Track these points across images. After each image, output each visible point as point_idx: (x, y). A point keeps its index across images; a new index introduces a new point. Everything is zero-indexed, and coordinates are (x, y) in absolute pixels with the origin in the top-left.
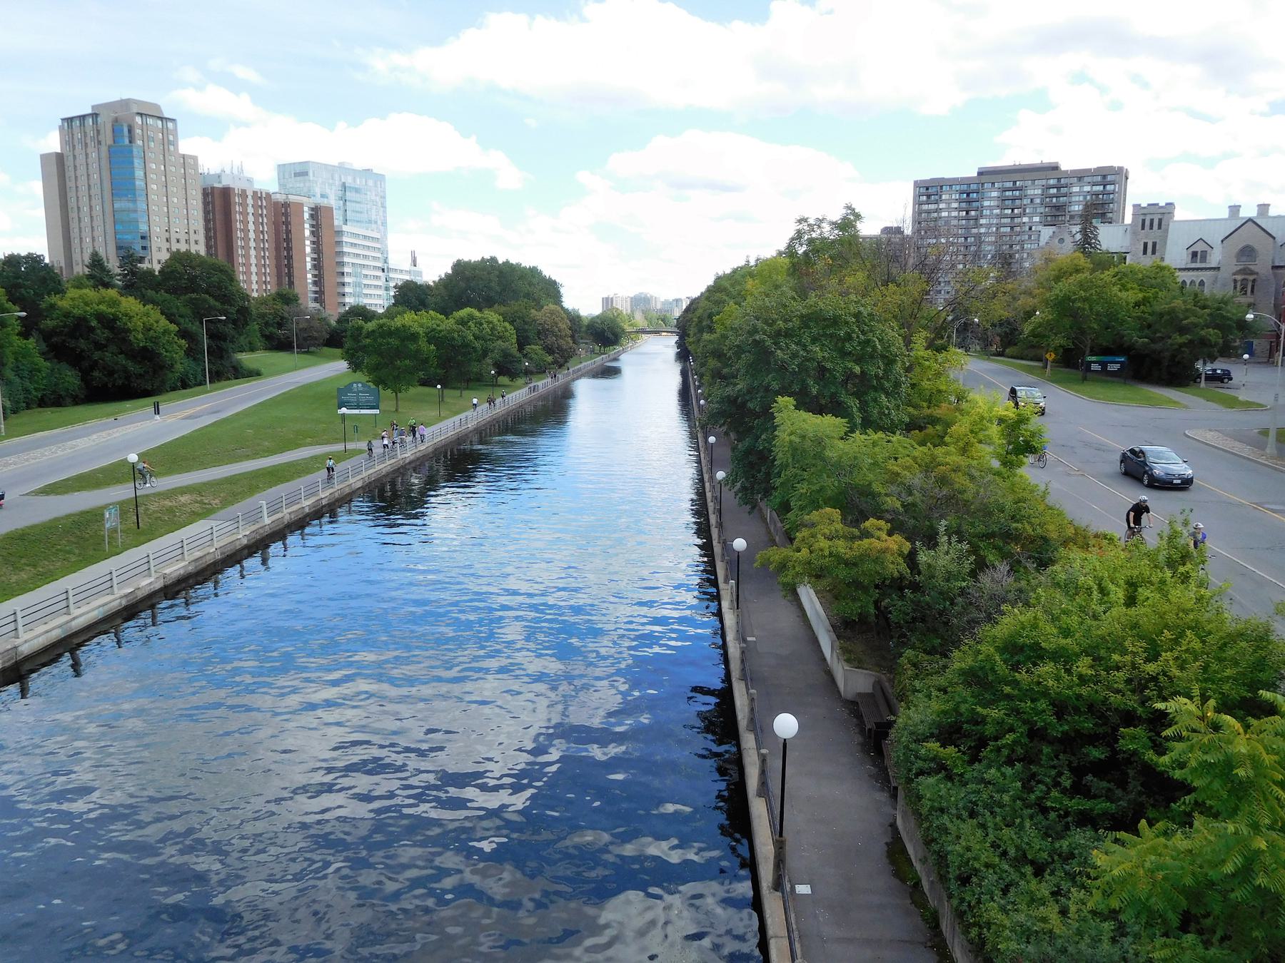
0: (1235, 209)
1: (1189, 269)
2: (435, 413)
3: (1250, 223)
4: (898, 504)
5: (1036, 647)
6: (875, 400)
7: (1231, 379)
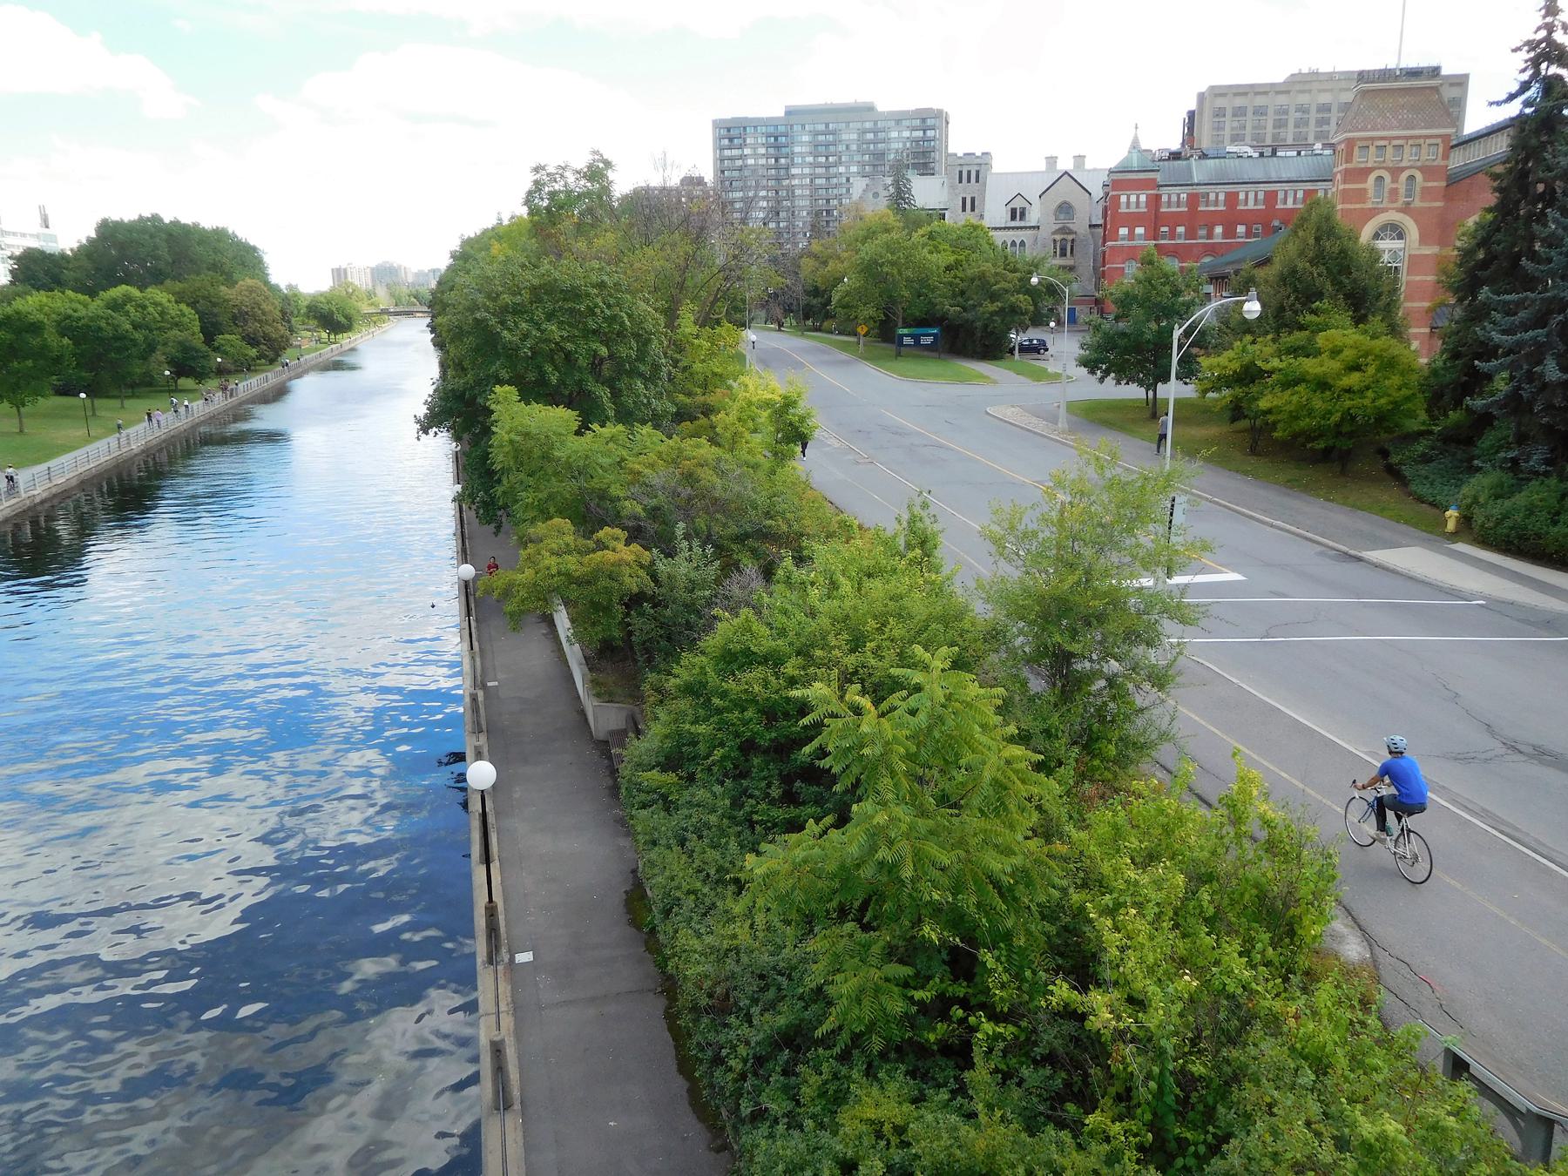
0: (1052, 161)
1: (1009, 228)
2: (82, 432)
3: (1066, 176)
4: (639, 509)
5: (747, 653)
6: (630, 388)
7: (1047, 350)
